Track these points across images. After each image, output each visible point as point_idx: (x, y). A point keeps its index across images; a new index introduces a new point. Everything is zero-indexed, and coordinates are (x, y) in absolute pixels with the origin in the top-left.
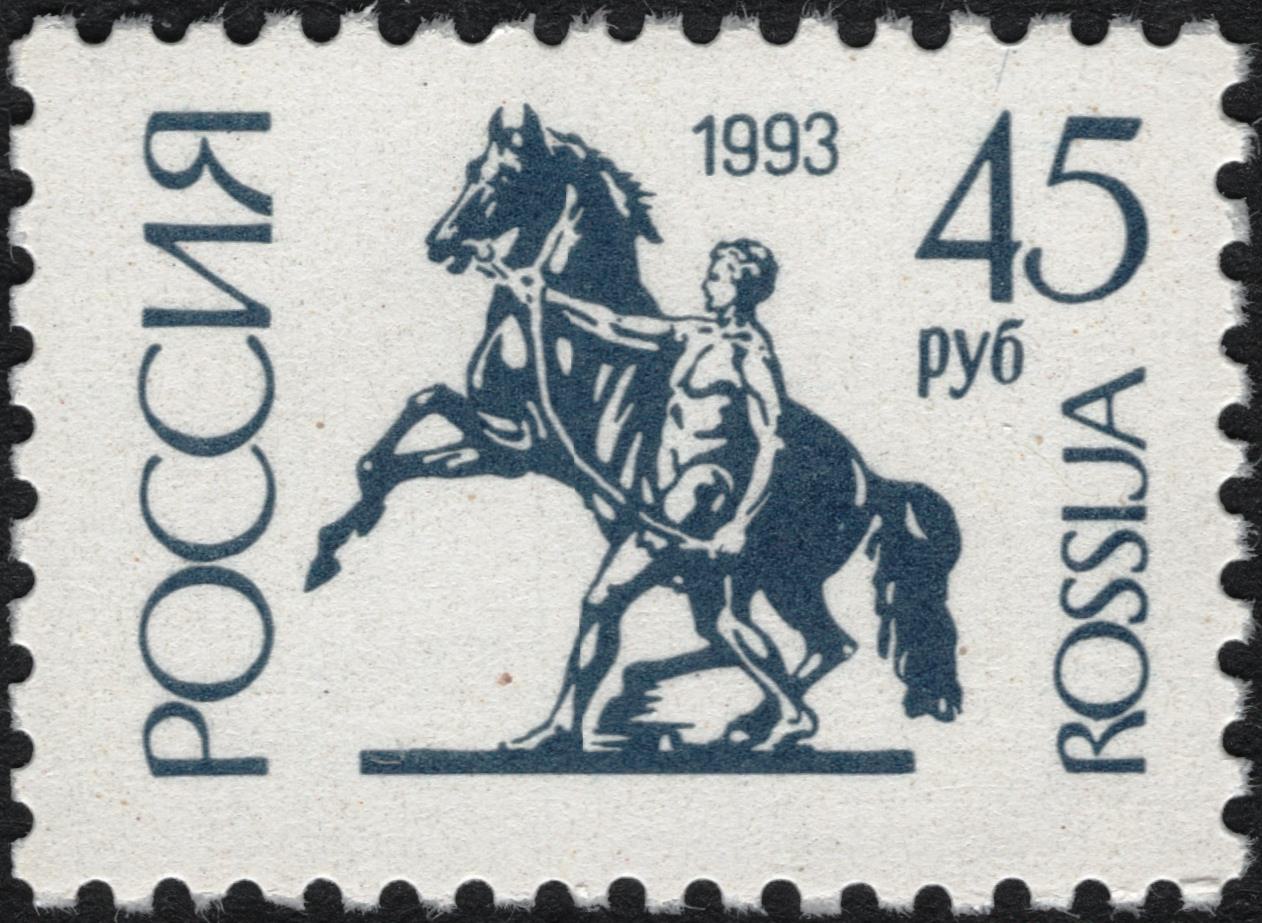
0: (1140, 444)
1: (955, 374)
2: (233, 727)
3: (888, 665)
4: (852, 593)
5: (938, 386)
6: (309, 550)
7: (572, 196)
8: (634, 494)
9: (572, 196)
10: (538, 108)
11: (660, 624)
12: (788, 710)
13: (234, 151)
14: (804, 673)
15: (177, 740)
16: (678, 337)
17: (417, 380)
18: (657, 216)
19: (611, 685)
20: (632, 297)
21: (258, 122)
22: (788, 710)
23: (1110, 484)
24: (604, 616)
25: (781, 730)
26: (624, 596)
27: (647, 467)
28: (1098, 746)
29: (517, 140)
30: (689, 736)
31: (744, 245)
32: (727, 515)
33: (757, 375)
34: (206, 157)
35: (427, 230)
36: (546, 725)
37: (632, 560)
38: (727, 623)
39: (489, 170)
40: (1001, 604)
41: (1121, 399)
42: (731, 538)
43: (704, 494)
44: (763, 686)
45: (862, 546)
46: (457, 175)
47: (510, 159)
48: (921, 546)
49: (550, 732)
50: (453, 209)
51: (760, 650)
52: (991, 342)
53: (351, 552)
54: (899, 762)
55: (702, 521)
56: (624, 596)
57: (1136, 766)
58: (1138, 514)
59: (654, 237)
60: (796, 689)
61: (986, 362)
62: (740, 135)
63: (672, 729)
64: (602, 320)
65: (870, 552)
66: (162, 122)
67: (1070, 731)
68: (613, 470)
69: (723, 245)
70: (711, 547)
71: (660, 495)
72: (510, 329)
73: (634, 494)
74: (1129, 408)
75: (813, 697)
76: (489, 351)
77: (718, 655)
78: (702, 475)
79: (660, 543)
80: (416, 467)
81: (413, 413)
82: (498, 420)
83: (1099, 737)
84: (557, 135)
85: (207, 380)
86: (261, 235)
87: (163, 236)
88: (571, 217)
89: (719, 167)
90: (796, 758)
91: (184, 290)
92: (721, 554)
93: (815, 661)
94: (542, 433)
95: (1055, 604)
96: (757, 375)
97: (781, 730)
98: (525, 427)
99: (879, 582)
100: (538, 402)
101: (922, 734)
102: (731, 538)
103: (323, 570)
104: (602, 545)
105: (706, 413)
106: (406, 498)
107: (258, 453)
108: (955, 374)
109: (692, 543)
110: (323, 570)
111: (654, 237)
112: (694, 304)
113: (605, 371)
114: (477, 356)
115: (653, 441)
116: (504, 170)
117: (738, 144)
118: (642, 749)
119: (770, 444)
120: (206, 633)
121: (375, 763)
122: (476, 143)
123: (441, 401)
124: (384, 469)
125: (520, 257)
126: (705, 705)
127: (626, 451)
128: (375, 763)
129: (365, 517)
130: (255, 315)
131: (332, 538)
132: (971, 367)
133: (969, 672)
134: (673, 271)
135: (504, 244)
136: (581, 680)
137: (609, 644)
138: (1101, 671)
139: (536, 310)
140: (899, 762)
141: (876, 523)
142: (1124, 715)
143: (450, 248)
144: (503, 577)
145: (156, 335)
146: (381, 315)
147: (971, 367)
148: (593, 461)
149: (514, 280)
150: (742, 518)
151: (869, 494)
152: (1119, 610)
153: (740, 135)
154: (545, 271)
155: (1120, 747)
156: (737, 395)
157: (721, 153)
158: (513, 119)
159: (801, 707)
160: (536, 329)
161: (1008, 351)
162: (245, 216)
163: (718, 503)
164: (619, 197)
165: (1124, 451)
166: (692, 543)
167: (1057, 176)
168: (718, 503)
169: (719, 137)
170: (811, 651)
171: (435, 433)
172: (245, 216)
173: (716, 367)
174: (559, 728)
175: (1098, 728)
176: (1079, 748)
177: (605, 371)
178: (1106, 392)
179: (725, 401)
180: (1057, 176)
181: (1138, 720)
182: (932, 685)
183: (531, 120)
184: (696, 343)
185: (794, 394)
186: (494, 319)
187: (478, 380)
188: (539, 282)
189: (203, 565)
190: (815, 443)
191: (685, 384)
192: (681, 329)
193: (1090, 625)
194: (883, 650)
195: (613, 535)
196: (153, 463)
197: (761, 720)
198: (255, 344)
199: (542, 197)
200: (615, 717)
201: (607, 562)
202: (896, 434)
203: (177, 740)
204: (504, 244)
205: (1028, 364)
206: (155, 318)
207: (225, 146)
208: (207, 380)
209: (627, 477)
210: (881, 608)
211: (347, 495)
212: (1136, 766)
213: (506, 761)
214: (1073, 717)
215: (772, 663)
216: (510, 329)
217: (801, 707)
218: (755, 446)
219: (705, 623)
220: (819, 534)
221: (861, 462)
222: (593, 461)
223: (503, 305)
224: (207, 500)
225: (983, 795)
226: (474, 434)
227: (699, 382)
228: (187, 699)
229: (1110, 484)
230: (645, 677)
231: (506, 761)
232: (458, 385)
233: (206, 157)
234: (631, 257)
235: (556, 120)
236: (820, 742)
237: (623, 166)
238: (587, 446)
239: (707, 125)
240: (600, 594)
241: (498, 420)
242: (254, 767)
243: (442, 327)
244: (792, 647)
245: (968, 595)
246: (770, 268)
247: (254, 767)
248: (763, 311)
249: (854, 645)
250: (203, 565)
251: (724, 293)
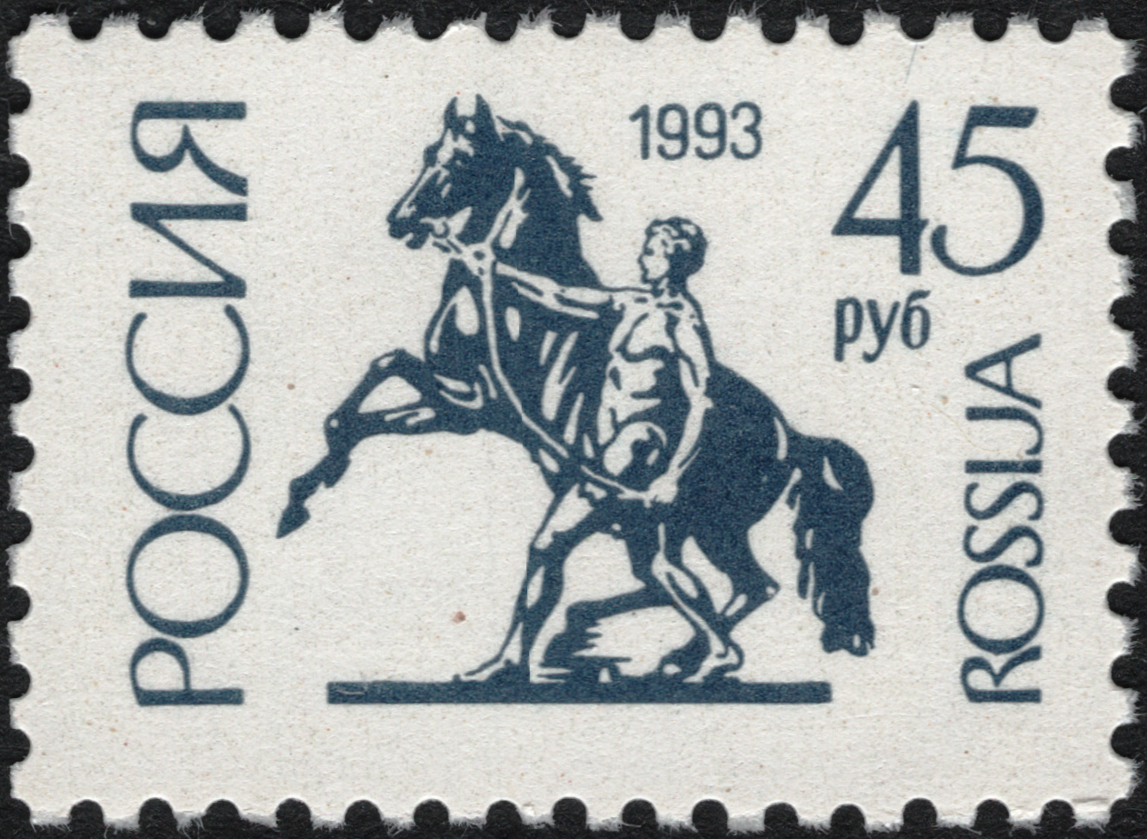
0: (1036, 403)
1: (868, 340)
2: (212, 661)
3: (807, 604)
4: (774, 539)
5: (853, 351)
6: (281, 500)
7: (520, 178)
8: (576, 449)
9: (520, 178)
10: (489, 98)
11: (600, 567)
12: (716, 645)
13: (212, 137)
14: (730, 612)
15: (161, 673)
16: (617, 306)
17: (380, 345)
18: (597, 196)
19: (556, 623)
20: (575, 270)
21: (235, 111)
22: (716, 645)
23: (1009, 440)
24: (549, 560)
25: (710, 664)
26: (567, 542)
27: (588, 425)
28: (998, 678)
29: (470, 127)
30: (626, 669)
31: (676, 223)
32: (661, 468)
33: (688, 341)
34: (187, 143)
35: (388, 209)
36: (497, 659)
37: (574, 509)
38: (661, 567)
39: (445, 155)
40: (909, 549)
41: (1019, 362)
42: (664, 489)
43: (640, 449)
44: (694, 624)
45: (784, 496)
46: (416, 159)
47: (464, 144)
48: (837, 496)
49: (500, 665)
51: (691, 590)
52: (901, 311)
53: (319, 502)
54: (817, 693)
55: (638, 474)
56: (567, 542)
57: (1032, 696)
58: (1034, 467)
59: (594, 215)
60: (724, 626)
61: (896, 329)
62: (673, 122)
63: (611, 663)
64: (547, 291)
65: (791, 502)
66: (147, 111)
67: (972, 664)
68: (557, 428)
69: (657, 223)
70: (647, 497)
71: (600, 450)
72: (463, 299)
73: (576, 449)
74: (1026, 371)
75: (739, 634)
76: (445, 319)
77: (652, 596)
78: (638, 432)
79: (600, 494)
80: (378, 424)
81: (375, 376)
82: (453, 382)
83: (999, 670)
84: (506, 123)
85: (188, 345)
86: (237, 213)
87: (148, 215)
88: (519, 198)
89: (653, 152)
90: (724, 689)
91: (167, 263)
92: (655, 504)
93: (741, 601)
94: (493, 394)
95: (959, 549)
96: (688, 341)
97: (710, 664)
98: (477, 388)
99: (799, 529)
100: (489, 366)
101: (838, 668)
102: (664, 489)
103: (293, 518)
104: (547, 496)
105: (642, 376)
106: (369, 453)
107: (234, 412)
108: (868, 340)
109: (629, 494)
110: (293, 518)
111: (594, 215)
112: (631, 276)
113: (550, 338)
114: (433, 323)
115: (593, 401)
116: (458, 154)
117: (671, 131)
118: (584, 681)
119: (699, 404)
120: (187, 575)
121: (340, 694)
122: (433, 130)
123: (401, 364)
124: (349, 427)
125: (473, 233)
126: (641, 641)
127: (569, 410)
128: (340, 694)
129: (331, 470)
130: (232, 286)
131: (302, 489)
132: (882, 334)
133: (880, 611)
134: (611, 247)
135: (459, 221)
136: (528, 618)
137: (554, 585)
138: (1001, 610)
139: (486, 280)
140: (817, 693)
141: (797, 475)
142: (1022, 649)
143: (409, 226)
144: (457, 525)
145: (142, 304)
146: (346, 286)
147: (882, 334)
148: (539, 419)
149: (467, 254)
150: (675, 471)
151: (790, 449)
152: (1017, 555)
153: (673, 122)
154: (496, 246)
155: (1018, 679)
156: (670, 359)
157: (655, 139)
158: (466, 108)
159: (728, 643)
160: (487, 299)
161: (916, 319)
162: (222, 197)
163: (653, 457)
164: (562, 179)
165: (1022, 410)
166: (629, 494)
168: (653, 457)
169: (653, 124)
170: (737, 592)
171: (395, 394)
172: (222, 197)
173: (651, 334)
174: (508, 662)
175: (998, 662)
176: (981, 680)
177: (550, 338)
178: (1005, 357)
179: (659, 364)
181: (1035, 654)
182: (847, 622)
183: (483, 109)
184: (633, 312)
185: (722, 358)
186: (449, 290)
188: (490, 257)
189: (185, 514)
190: (740, 403)
191: (622, 349)
192: (619, 299)
193: (991, 569)
194: (802, 591)
195: (557, 486)
196: (139, 421)
197: (692, 654)
198: (231, 313)
199: (493, 179)
200: (559, 652)
201: (551, 511)
202: (815, 395)
203: (161, 673)
204: (459, 221)
205: (934, 330)
206: (141, 289)
207: (205, 132)
208: (188, 345)
209: (570, 434)
210: (801, 553)
211: (315, 450)
212: (1032, 696)
213: (460, 692)
214: (975, 652)
216: (463, 299)
217: (728, 643)
218: (686, 406)
219: (641, 566)
220: (744, 486)
221: (782, 420)
222: (539, 419)
223: (457, 277)
224: (188, 455)
225: (893, 722)
226: (431, 395)
227: (635, 347)
228: (170, 635)
229: (1009, 440)
230: (587, 615)
231: (460, 692)
232: (416, 350)
233: (187, 143)
234: (574, 234)
235: (505, 109)
236: (746, 674)
237: (566, 151)
238: (534, 405)
239: (642, 114)
240: (545, 540)
241: (453, 382)
242: (231, 697)
243: (402, 298)
244: (720, 588)
245: (879, 541)
246: (700, 243)
247: (231, 697)
248: (693, 283)
249: (776, 586)
250: (185, 514)
251: (658, 266)
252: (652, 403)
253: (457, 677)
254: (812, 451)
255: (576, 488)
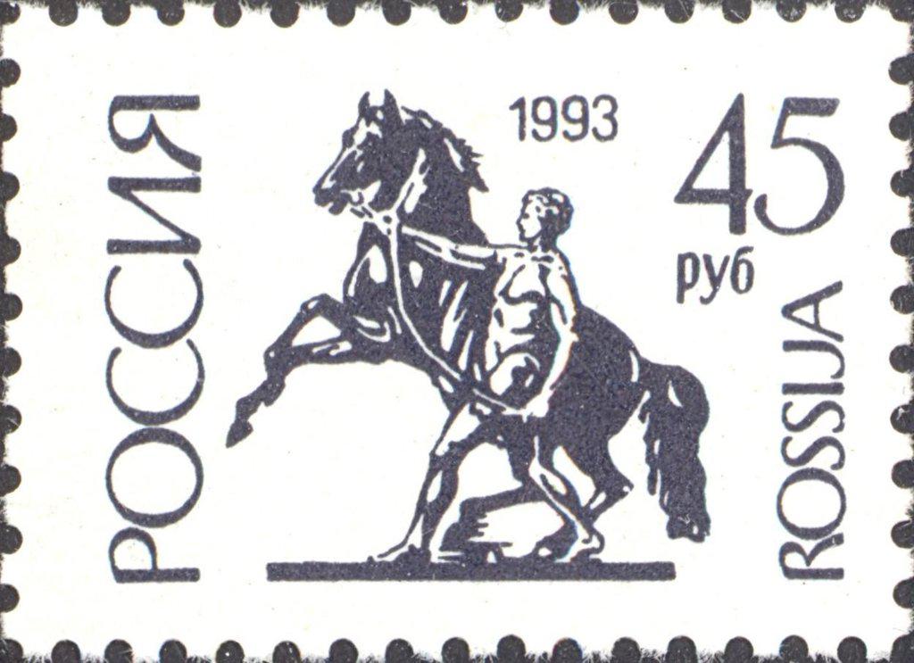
0: (839, 338)
2: (173, 546)
4: (629, 448)
11: (487, 470)
12: (582, 532)
14: (593, 506)
15: (133, 555)
16: (500, 260)
19: (452, 516)
22: (582, 532)
23: (818, 367)
24: (446, 465)
27: (477, 355)
28: (809, 559)
30: (507, 552)
31: (547, 192)
32: (536, 389)
37: (467, 423)
38: (536, 470)
39: (359, 138)
41: (824, 304)
42: (538, 407)
43: (518, 374)
44: (564, 517)
45: (637, 412)
47: (375, 129)
48: (679, 410)
49: (405, 549)
50: (332, 168)
53: (261, 418)
54: (663, 571)
55: (519, 394)
57: (837, 574)
59: (482, 187)
63: (495, 547)
64: (444, 248)
66: (121, 103)
67: (788, 548)
68: (452, 357)
69: (531, 193)
70: (524, 413)
71: (487, 375)
72: (375, 254)
76: (360, 268)
77: (528, 492)
78: (518, 360)
80: (307, 355)
83: (809, 552)
86: (193, 185)
87: (122, 187)
90: (590, 569)
93: (602, 497)
94: (399, 330)
96: (559, 289)
99: (649, 438)
101: (679, 551)
102: (538, 407)
103: (239, 431)
104: (445, 413)
105: (520, 315)
106: (301, 378)
110: (239, 431)
111: (482, 187)
112: (514, 238)
113: (447, 285)
114: (353, 270)
115: (482, 337)
116: (370, 136)
117: (542, 117)
118: (474, 561)
119: (567, 338)
120: (154, 477)
121: (279, 572)
122: (351, 116)
123: (324, 306)
124: (284, 357)
125: (381, 203)
126: (519, 529)
128: (279, 572)
129: (269, 392)
130: (189, 244)
131: (246, 407)
132: (715, 281)
134: (495, 212)
136: (428, 513)
139: (393, 239)
140: (663, 571)
143: (331, 196)
144: (375, 433)
147: (715, 281)
148: (438, 351)
149: (377, 219)
150: (547, 392)
156: (544, 302)
157: (530, 125)
158: (377, 100)
161: (743, 268)
162: (183, 172)
164: (456, 158)
166: (509, 411)
167: (778, 142)
171: (320, 330)
172: (183, 172)
173: (528, 281)
174: (412, 547)
175: (808, 546)
176: (795, 561)
177: (447, 285)
178: (814, 300)
179: (534, 306)
180: (778, 142)
181: (839, 539)
184: (511, 266)
185: (587, 301)
186: (363, 247)
187: (351, 292)
188: (396, 221)
189: (153, 428)
190: (601, 338)
191: (504, 293)
195: (454, 404)
199: (398, 155)
202: (660, 332)
203: (133, 555)
206: (116, 247)
207: (165, 119)
208: (154, 291)
209: (463, 362)
211: (258, 376)
212: (837, 574)
215: (570, 498)
216: (375, 254)
217: (592, 531)
218: (555, 340)
221: (637, 354)
222: (438, 351)
223: (370, 237)
224: (155, 380)
226: (349, 331)
227: (515, 292)
228: (140, 526)
229: (818, 367)
230: (476, 510)
232: (338, 296)
235: (408, 100)
236: (606, 557)
238: (434, 339)
243: (326, 252)
244: (585, 487)
245: (713, 448)
246: (566, 208)
248: (562, 242)
250: (153, 428)
251: (533, 227)
252: (529, 337)
253: (370, 559)
254: (656, 375)
255: (466, 408)
